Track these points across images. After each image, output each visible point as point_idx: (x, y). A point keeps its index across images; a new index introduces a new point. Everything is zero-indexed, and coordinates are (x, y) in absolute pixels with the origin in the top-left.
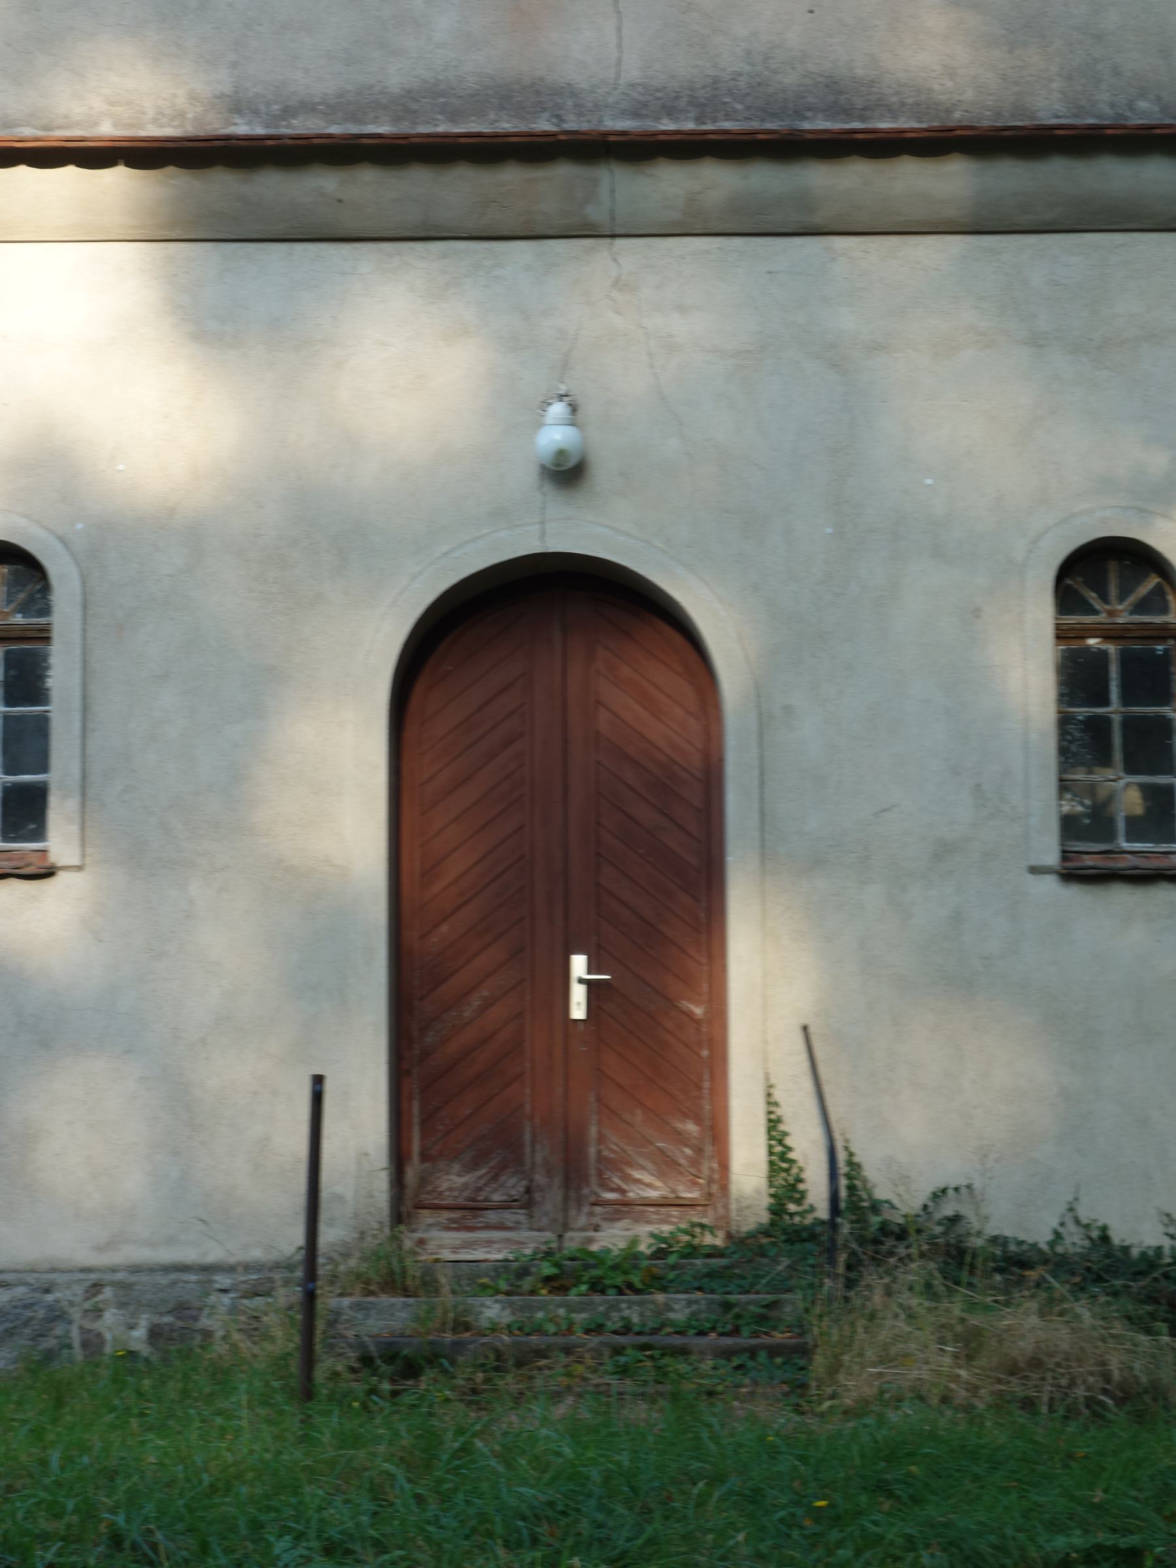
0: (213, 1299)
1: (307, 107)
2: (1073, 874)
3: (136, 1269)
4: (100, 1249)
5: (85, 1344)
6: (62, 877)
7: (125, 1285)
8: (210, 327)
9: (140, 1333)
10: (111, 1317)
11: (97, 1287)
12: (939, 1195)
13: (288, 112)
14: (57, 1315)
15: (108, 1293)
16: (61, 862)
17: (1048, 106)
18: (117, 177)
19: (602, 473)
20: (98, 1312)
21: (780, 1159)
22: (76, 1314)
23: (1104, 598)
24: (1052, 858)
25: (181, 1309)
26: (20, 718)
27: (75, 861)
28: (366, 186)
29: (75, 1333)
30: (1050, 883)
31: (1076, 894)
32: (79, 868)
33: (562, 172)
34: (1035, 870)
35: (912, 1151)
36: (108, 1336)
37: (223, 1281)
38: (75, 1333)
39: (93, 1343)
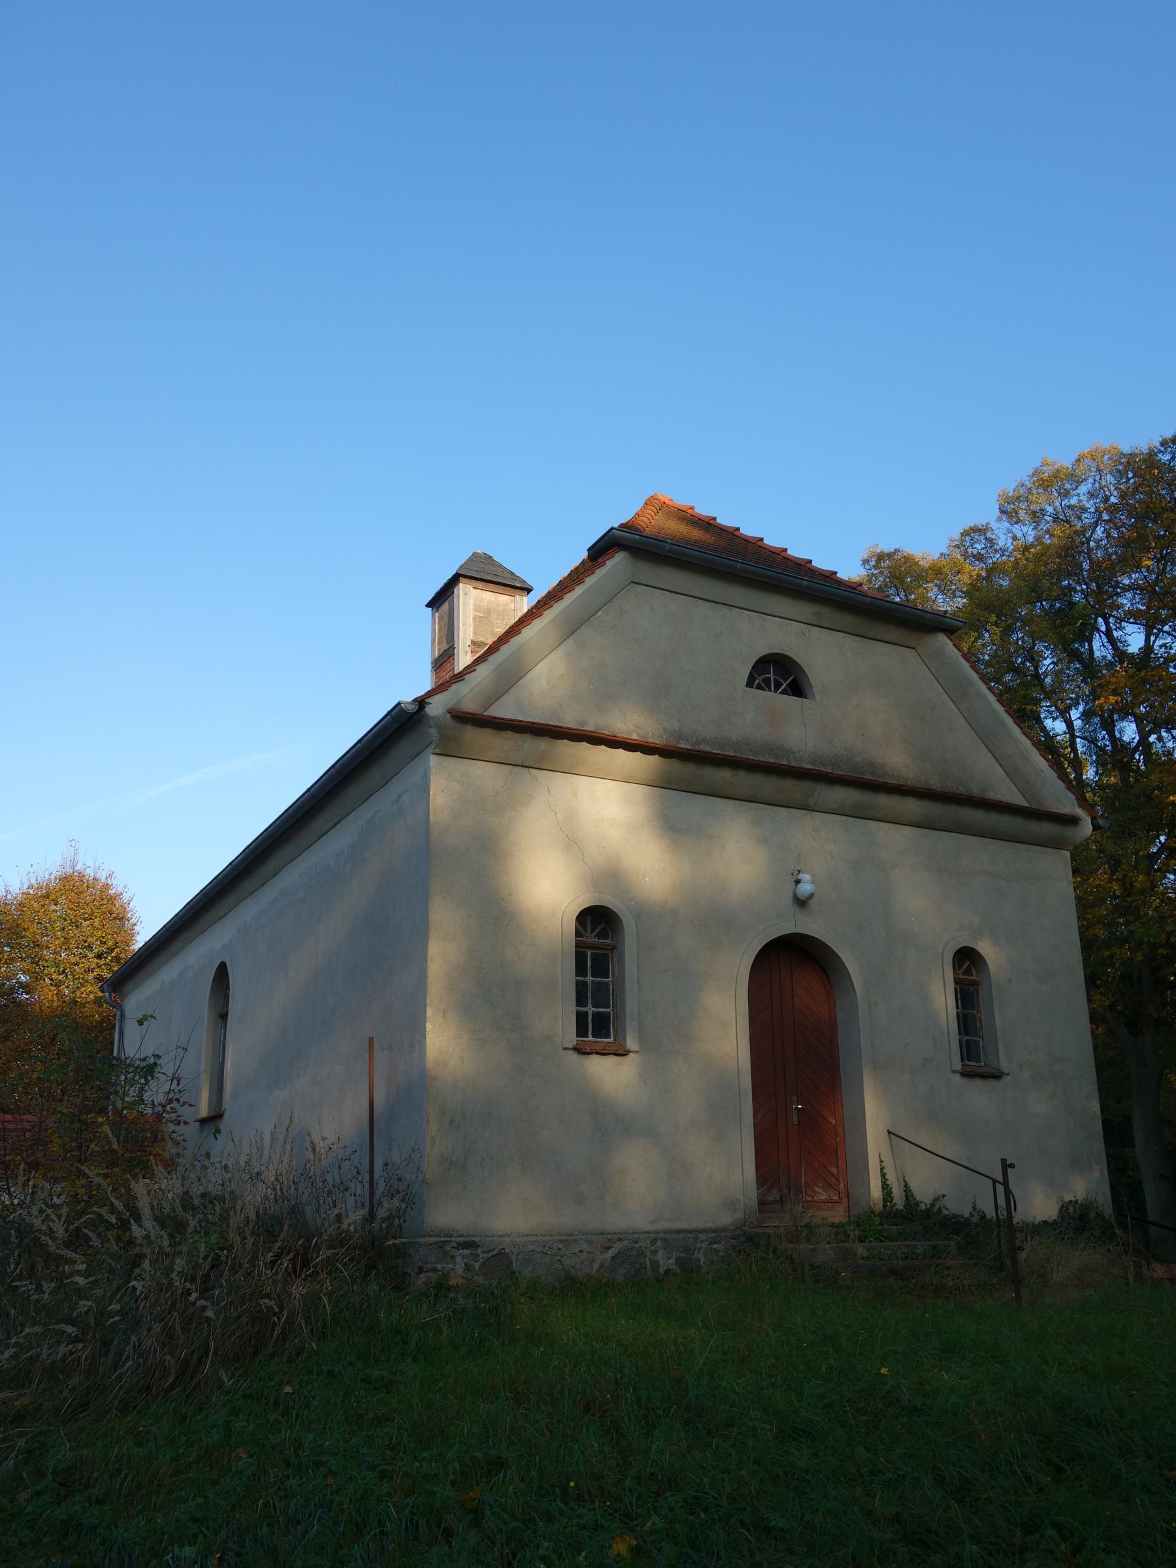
0: (698, 1245)
1: (704, 741)
2: (967, 1074)
3: (665, 1232)
4: (651, 1223)
5: (652, 1266)
6: (631, 1055)
7: (666, 1239)
8: (671, 827)
9: (672, 1261)
10: (660, 1254)
11: (654, 1241)
12: (937, 1199)
13: (698, 742)
14: (641, 1253)
15: (659, 1243)
16: (632, 1049)
17: (935, 784)
18: (654, 759)
19: (813, 903)
20: (655, 1252)
21: (885, 1186)
22: (648, 1253)
23: (593, 931)
24: (959, 1067)
25: (687, 1249)
26: (598, 983)
27: (637, 1049)
28: (744, 781)
29: (648, 1262)
30: (957, 1077)
31: (965, 1081)
32: (637, 1052)
33: (807, 784)
34: (954, 1072)
35: (928, 1181)
36: (661, 1262)
37: (702, 1237)
38: (648, 1262)
39: (655, 1265)
